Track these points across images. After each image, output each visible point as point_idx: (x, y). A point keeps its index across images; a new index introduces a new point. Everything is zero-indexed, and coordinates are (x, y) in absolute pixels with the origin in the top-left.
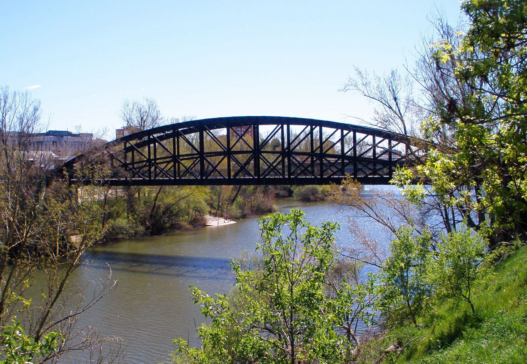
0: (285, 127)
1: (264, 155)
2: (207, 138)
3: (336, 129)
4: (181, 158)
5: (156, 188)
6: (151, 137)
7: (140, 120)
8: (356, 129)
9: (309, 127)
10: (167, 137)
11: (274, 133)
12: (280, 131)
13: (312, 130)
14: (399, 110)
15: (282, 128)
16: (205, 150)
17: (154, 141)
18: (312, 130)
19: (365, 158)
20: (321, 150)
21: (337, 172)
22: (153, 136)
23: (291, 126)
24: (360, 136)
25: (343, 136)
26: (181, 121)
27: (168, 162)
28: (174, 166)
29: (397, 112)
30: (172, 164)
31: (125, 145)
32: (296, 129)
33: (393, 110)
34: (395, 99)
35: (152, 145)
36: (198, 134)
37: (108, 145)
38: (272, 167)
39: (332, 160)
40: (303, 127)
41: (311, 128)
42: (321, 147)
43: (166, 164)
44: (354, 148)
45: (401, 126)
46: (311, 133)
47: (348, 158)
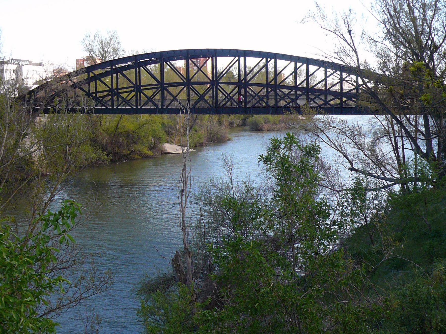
0: (242, 59)
1: (221, 85)
2: (167, 68)
3: (301, 64)
4: (142, 88)
5: (116, 117)
6: (114, 68)
7: (102, 52)
8: (308, 61)
9: (264, 60)
10: (129, 67)
11: (230, 66)
12: (237, 64)
13: (267, 62)
14: (353, 43)
15: (239, 60)
16: (165, 80)
17: (117, 71)
18: (267, 62)
19: (316, 89)
20: (276, 82)
21: (290, 102)
22: (116, 67)
23: (248, 59)
24: (312, 68)
25: (296, 69)
26: (140, 53)
27: (131, 92)
28: (136, 95)
29: (352, 45)
30: (133, 93)
31: (89, 75)
32: (252, 62)
33: (347, 42)
34: (350, 32)
35: (114, 75)
36: (157, 65)
37: (70, 75)
38: (229, 97)
39: (286, 91)
40: (258, 59)
41: (267, 60)
42: (275, 78)
43: (128, 93)
44: (307, 79)
45: (355, 58)
46: (266, 66)
47: (302, 89)
